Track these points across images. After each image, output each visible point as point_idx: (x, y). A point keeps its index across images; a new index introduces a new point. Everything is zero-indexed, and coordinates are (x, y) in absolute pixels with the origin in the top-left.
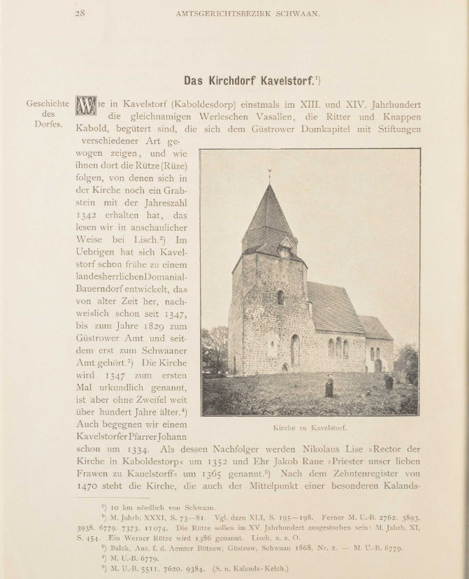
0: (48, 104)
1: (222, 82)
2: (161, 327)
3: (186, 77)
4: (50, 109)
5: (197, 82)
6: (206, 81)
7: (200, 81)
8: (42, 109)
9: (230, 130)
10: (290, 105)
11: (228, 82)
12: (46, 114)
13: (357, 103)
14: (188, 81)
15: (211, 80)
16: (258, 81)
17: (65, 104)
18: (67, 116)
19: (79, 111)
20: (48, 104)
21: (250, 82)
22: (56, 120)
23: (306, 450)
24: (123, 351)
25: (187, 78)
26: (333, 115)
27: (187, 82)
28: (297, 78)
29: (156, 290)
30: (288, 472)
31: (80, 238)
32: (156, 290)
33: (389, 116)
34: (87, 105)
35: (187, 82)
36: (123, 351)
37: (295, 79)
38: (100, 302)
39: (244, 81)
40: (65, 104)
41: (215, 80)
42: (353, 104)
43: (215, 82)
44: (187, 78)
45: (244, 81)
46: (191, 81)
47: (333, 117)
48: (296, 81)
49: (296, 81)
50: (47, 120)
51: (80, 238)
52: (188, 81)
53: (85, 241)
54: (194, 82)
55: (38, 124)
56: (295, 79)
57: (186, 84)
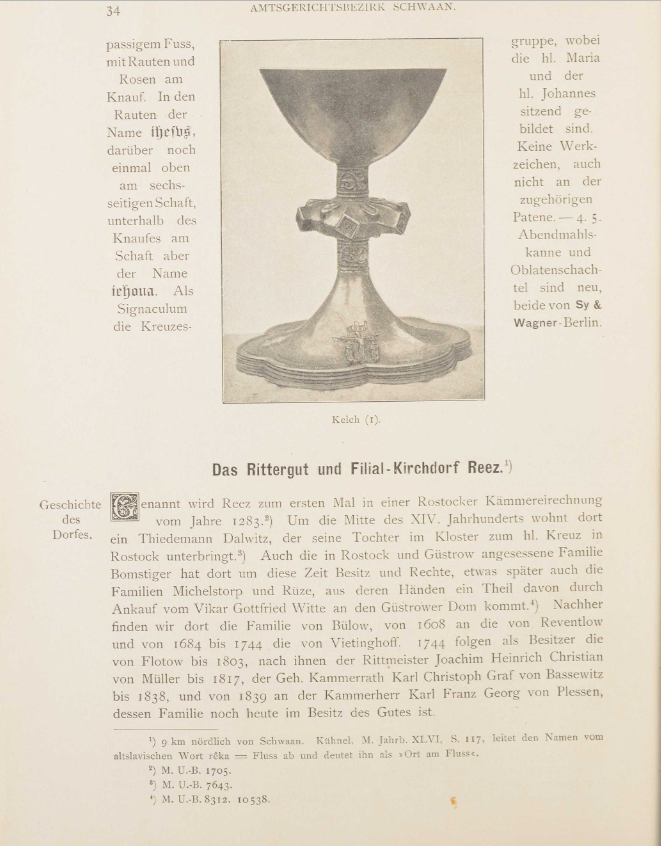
0: (71, 505)
1: (412, 470)
2: (263, 697)
3: (214, 465)
4: (73, 513)
5: (230, 472)
6: (242, 470)
7: (235, 471)
8: (63, 513)
9: (188, 627)
10: (131, 593)
11: (421, 469)
12: (67, 520)
13: (426, 517)
14: (218, 470)
15: (397, 467)
16: (463, 467)
17: (97, 506)
18: (99, 522)
19: (117, 517)
20: (71, 505)
21: (452, 469)
22: (82, 528)
23: (157, 275)
24: (494, 537)
25: (217, 467)
26: (372, 658)
27: (217, 472)
28: (273, 466)
29: (465, 503)
30: (163, 271)
31: (565, 143)
32: (465, 503)
33: (121, 238)
34: (125, 506)
35: (217, 472)
36: (494, 537)
37: (269, 467)
38: (505, 642)
39: (443, 469)
40: (97, 506)
41: (402, 468)
42: (420, 519)
43: (402, 471)
44: (217, 467)
45: (443, 469)
46: (222, 471)
47: (372, 661)
48: (272, 470)
49: (272, 470)
50: (71, 528)
51: (565, 143)
52: (218, 470)
53: (573, 148)
54: (226, 472)
55: (57, 535)
56: (269, 467)
57: (214, 474)
